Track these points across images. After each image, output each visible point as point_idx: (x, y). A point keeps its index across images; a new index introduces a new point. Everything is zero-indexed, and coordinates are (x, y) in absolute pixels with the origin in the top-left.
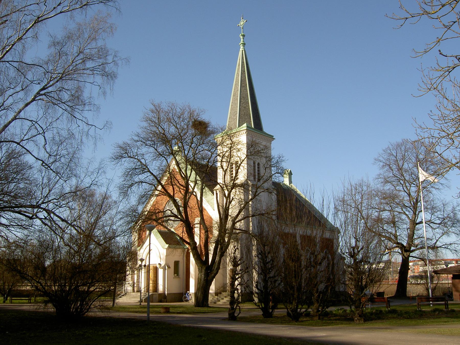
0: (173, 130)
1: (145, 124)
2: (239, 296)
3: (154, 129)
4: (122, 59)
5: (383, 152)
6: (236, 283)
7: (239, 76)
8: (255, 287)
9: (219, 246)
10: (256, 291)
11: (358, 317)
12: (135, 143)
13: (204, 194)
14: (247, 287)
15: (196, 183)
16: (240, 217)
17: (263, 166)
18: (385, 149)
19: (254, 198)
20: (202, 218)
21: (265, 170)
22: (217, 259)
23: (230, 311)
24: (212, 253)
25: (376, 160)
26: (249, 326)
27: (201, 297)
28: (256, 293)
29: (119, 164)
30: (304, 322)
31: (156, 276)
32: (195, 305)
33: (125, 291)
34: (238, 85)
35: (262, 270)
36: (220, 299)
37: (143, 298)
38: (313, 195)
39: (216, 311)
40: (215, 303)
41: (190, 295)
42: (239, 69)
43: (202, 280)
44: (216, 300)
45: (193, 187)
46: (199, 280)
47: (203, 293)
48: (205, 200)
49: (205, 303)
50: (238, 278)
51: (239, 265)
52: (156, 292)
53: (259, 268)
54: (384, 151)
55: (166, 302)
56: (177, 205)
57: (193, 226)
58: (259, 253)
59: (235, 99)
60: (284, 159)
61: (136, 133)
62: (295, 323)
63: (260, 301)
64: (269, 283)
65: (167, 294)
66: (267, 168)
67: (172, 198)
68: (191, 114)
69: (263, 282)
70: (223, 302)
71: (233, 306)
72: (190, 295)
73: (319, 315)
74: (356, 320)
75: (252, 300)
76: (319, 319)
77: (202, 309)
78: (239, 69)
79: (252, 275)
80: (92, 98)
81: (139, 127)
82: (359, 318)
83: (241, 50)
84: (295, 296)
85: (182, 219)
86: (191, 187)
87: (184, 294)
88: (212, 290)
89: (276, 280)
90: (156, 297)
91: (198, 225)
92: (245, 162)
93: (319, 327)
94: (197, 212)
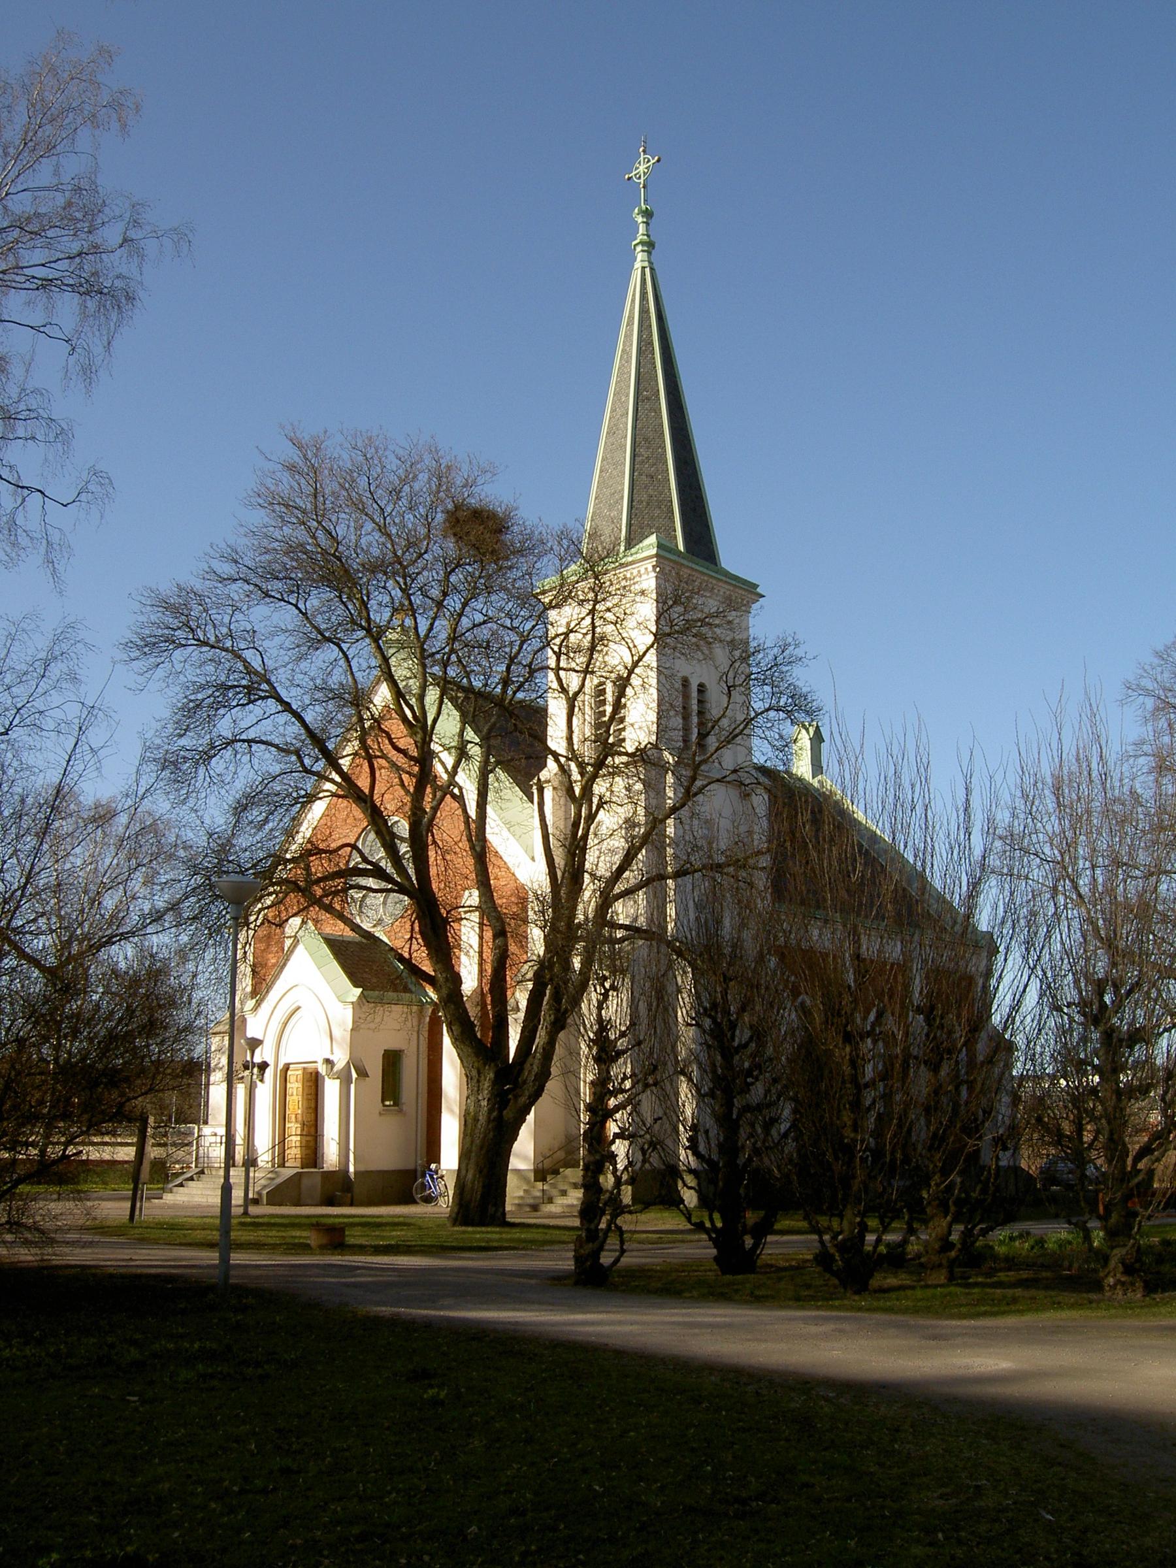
0: (372, 543)
1: (259, 518)
2: (618, 1182)
3: (301, 535)
4: (160, 233)
5: (1156, 661)
6: (612, 1128)
7: (629, 361)
8: (687, 1148)
9: (548, 992)
10: (692, 1163)
11: (1118, 1275)
12: (220, 589)
13: (491, 796)
14: (653, 1145)
15: (462, 753)
16: (631, 877)
17: (721, 678)
18: (1162, 648)
19: (683, 806)
20: (482, 884)
21: (729, 695)
22: (541, 1037)
23: (581, 1247)
24: (521, 1015)
25: (1129, 688)
26: (656, 1318)
27: (478, 1186)
28: (691, 1171)
29: (160, 672)
30: (893, 1295)
31: (313, 1105)
32: (454, 1215)
33: (201, 1160)
34: (628, 395)
35: (717, 1080)
36: (554, 1192)
37: (265, 1187)
38: (926, 770)
39: (532, 1242)
40: (535, 1208)
41: (442, 1177)
42: (628, 336)
43: (482, 1118)
44: (538, 1197)
45: (450, 767)
46: (470, 1121)
47: (485, 1171)
48: (496, 818)
49: (491, 1210)
50: (617, 1108)
51: (620, 1054)
52: (315, 1167)
53: (705, 1071)
54: (1158, 655)
55: (351, 1205)
56: (384, 829)
57: (448, 912)
58: (705, 1009)
59: (614, 448)
60: (799, 652)
61: (223, 546)
62: (856, 1298)
63: (704, 1201)
64: (743, 1133)
65: (356, 1173)
66: (734, 686)
67: (365, 802)
68: (441, 476)
69: (721, 1126)
70: (562, 1206)
71: (593, 1226)
72: (442, 1177)
73: (952, 1263)
74: (1113, 1287)
75: (673, 1201)
76: (951, 1278)
77: (479, 1233)
78: (628, 336)
79: (673, 1099)
80: (42, 394)
81: (242, 530)
82: (1123, 1279)
83: (638, 265)
84: (856, 1185)
85: (406, 883)
86: (443, 764)
87: (419, 1174)
88: (525, 1158)
89: (771, 1118)
90: (313, 1183)
91: (475, 917)
92: (651, 658)
93: (965, 1323)
94: (465, 863)
